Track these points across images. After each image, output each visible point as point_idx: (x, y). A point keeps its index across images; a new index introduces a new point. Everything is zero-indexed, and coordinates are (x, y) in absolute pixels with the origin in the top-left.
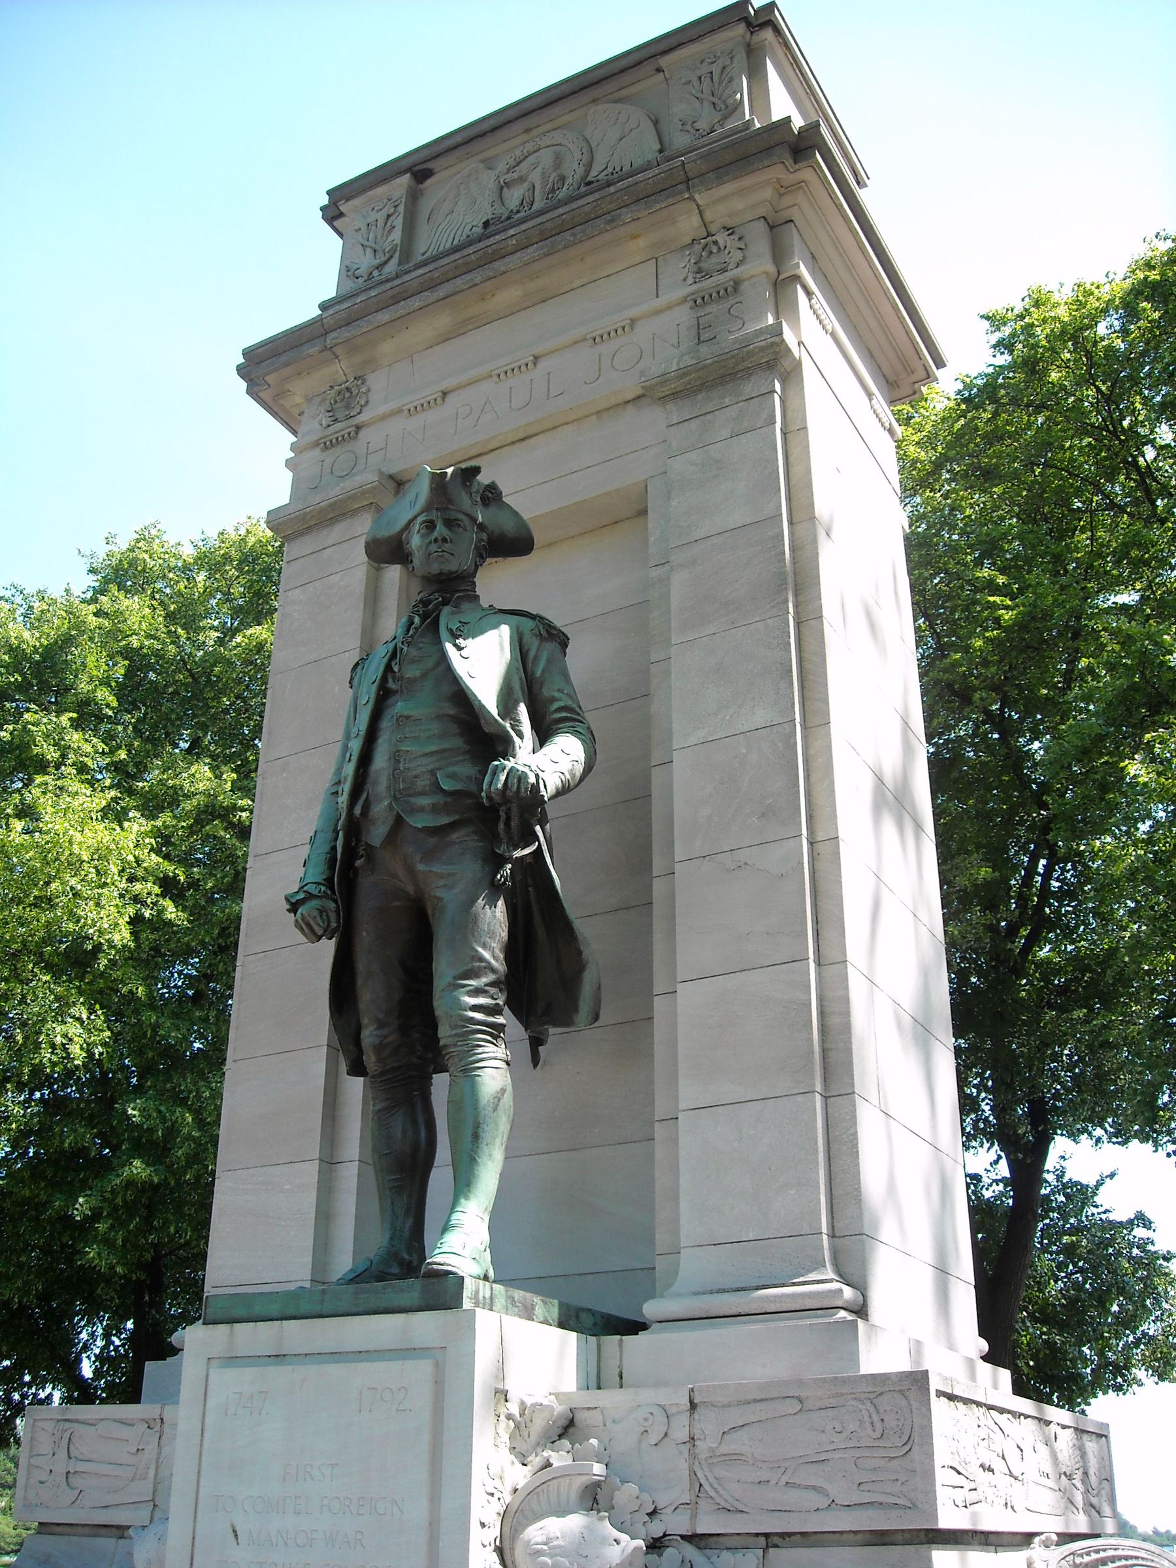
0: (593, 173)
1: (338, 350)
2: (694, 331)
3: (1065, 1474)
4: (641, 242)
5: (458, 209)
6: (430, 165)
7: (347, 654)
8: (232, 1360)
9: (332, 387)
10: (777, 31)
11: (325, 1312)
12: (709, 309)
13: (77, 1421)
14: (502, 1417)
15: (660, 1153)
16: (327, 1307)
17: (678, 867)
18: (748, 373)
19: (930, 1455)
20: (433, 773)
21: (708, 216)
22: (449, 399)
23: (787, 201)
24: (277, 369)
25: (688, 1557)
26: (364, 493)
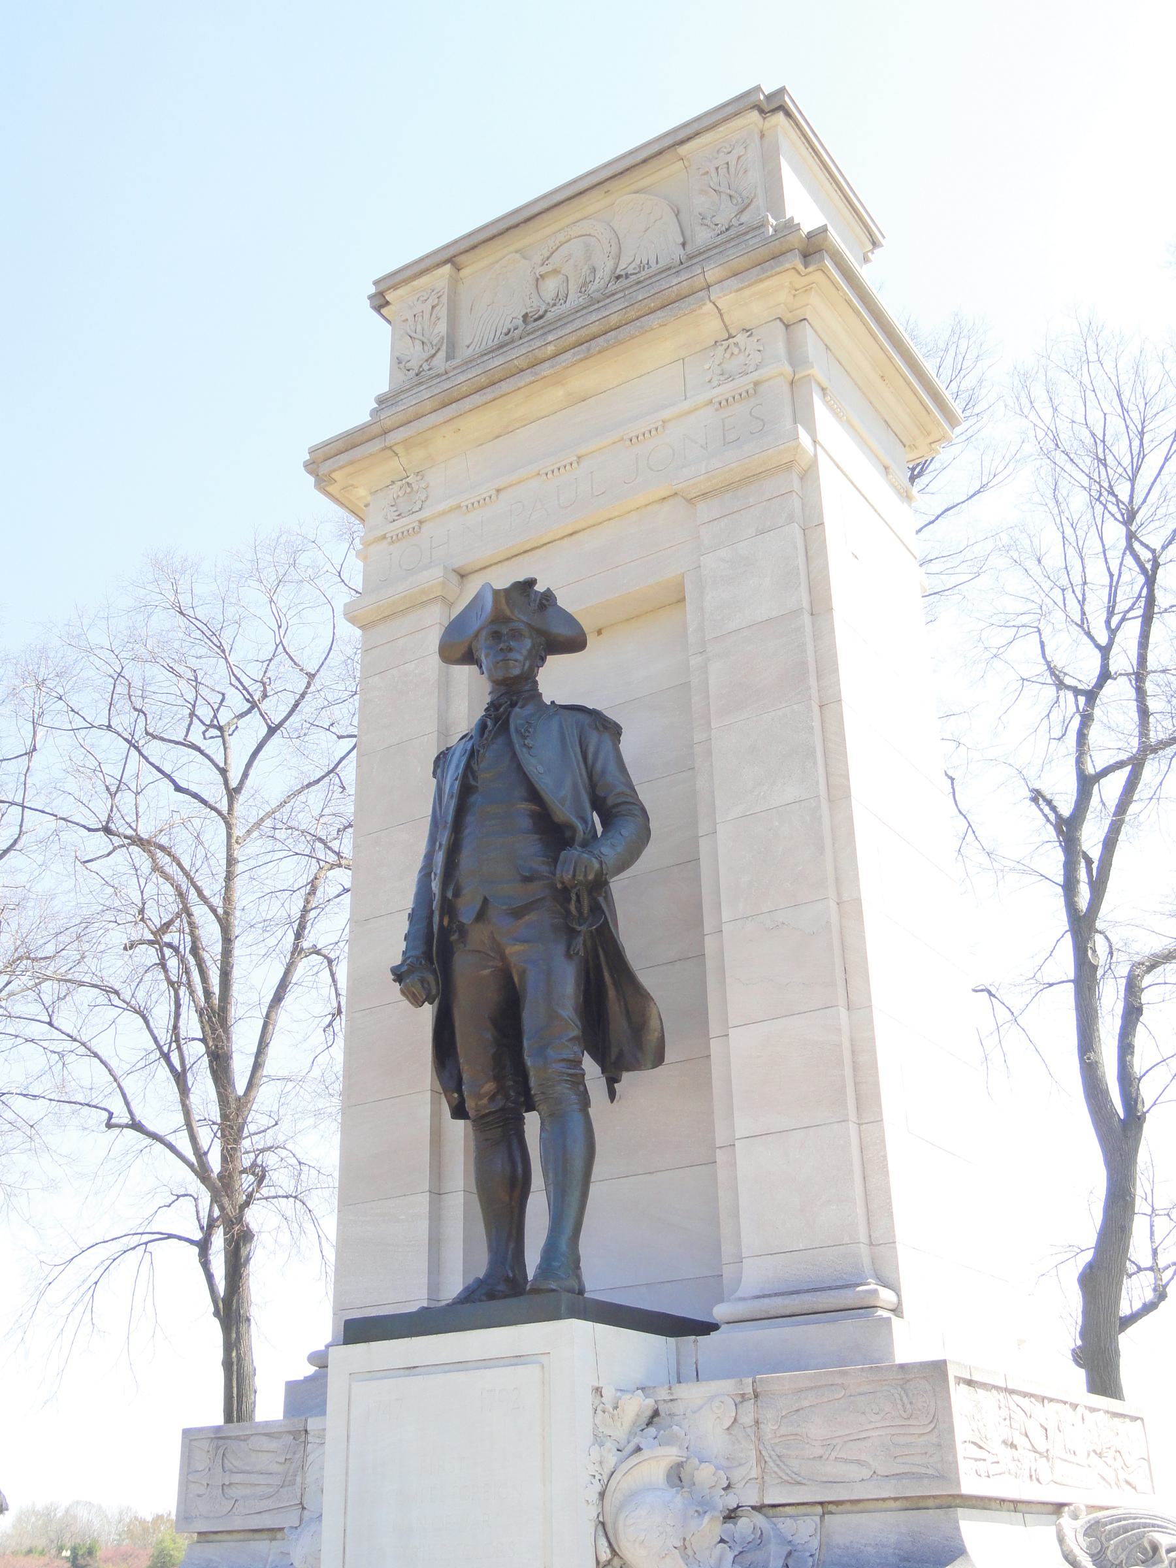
0: (622, 266)
1: (400, 450)
3: (1095, 1451)
5: (497, 296)
7: (426, 738)
9: (393, 482)
10: (788, 114)
14: (599, 1411)
15: (722, 1175)
17: (725, 927)
19: (951, 1431)
24: (341, 468)
25: (758, 1525)
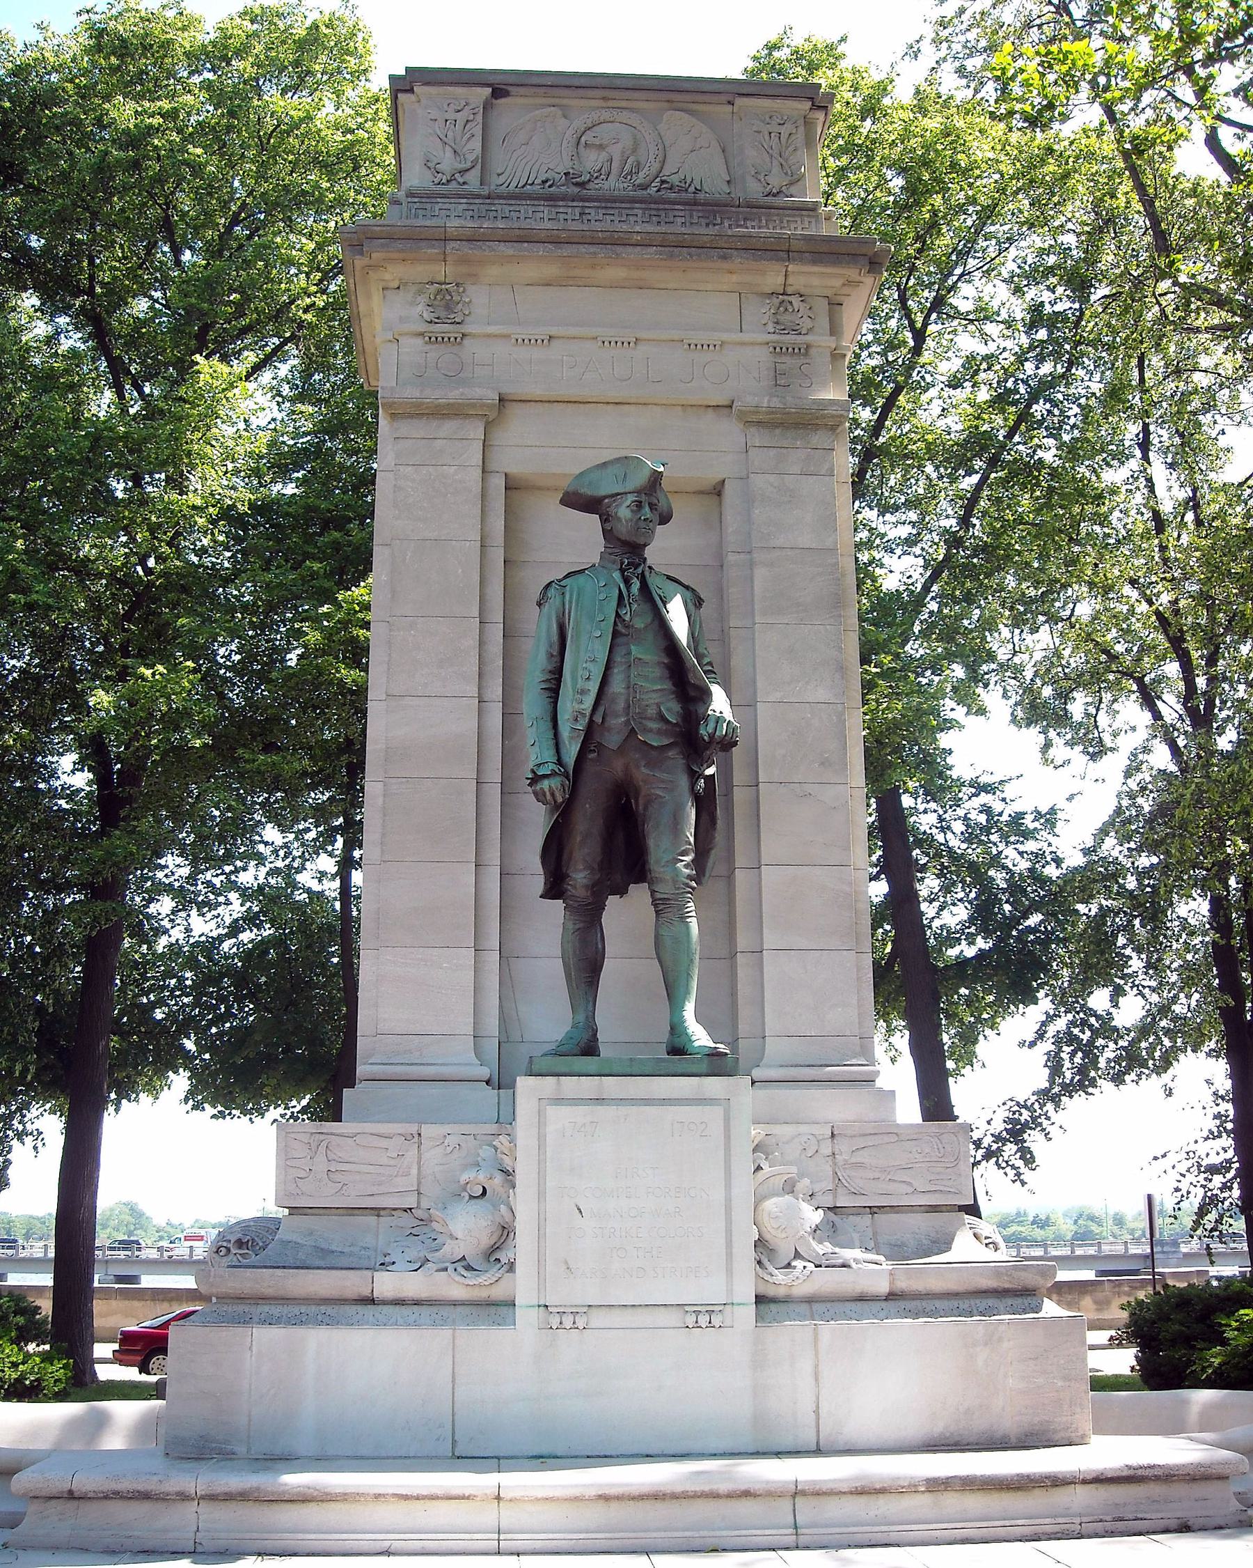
2: (772, 374)
4: (734, 278)
6: (510, 88)
8: (559, 1101)
11: (615, 1071)
12: (784, 359)
13: (332, 1134)
16: (635, 1070)
18: (816, 427)
20: (658, 705)
21: (790, 281)
22: (554, 343)
23: (846, 290)
26: (483, 405)
